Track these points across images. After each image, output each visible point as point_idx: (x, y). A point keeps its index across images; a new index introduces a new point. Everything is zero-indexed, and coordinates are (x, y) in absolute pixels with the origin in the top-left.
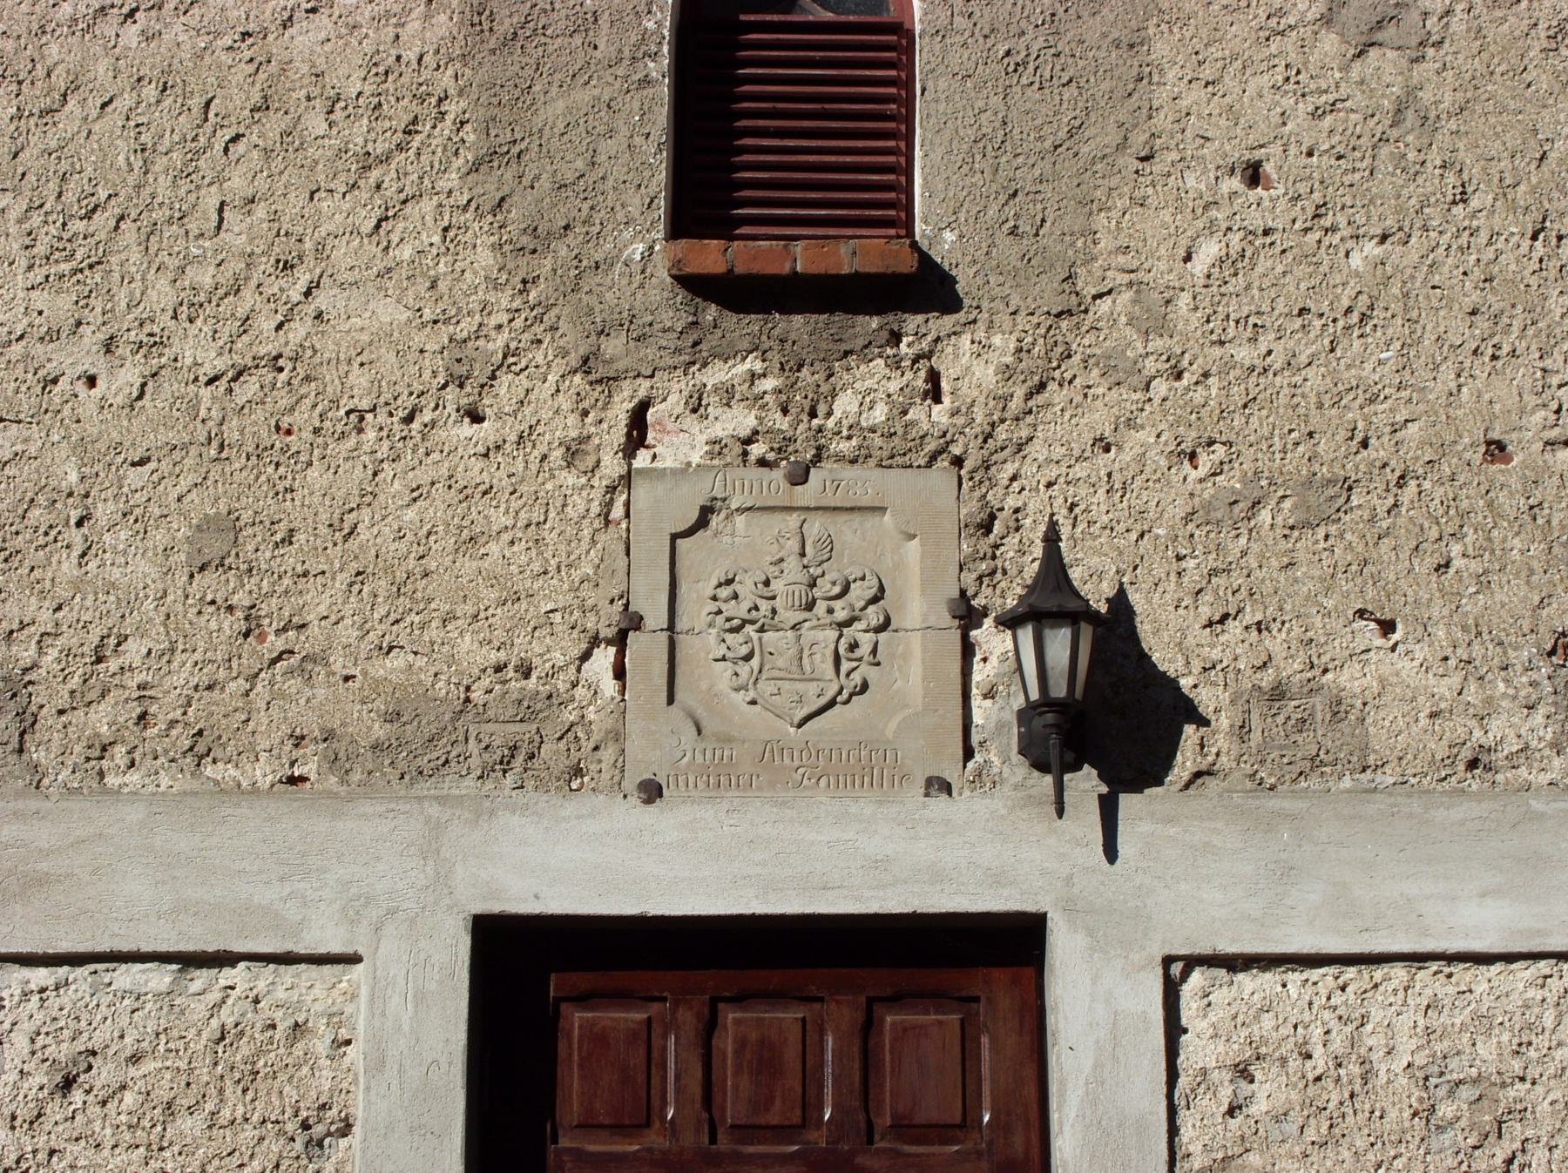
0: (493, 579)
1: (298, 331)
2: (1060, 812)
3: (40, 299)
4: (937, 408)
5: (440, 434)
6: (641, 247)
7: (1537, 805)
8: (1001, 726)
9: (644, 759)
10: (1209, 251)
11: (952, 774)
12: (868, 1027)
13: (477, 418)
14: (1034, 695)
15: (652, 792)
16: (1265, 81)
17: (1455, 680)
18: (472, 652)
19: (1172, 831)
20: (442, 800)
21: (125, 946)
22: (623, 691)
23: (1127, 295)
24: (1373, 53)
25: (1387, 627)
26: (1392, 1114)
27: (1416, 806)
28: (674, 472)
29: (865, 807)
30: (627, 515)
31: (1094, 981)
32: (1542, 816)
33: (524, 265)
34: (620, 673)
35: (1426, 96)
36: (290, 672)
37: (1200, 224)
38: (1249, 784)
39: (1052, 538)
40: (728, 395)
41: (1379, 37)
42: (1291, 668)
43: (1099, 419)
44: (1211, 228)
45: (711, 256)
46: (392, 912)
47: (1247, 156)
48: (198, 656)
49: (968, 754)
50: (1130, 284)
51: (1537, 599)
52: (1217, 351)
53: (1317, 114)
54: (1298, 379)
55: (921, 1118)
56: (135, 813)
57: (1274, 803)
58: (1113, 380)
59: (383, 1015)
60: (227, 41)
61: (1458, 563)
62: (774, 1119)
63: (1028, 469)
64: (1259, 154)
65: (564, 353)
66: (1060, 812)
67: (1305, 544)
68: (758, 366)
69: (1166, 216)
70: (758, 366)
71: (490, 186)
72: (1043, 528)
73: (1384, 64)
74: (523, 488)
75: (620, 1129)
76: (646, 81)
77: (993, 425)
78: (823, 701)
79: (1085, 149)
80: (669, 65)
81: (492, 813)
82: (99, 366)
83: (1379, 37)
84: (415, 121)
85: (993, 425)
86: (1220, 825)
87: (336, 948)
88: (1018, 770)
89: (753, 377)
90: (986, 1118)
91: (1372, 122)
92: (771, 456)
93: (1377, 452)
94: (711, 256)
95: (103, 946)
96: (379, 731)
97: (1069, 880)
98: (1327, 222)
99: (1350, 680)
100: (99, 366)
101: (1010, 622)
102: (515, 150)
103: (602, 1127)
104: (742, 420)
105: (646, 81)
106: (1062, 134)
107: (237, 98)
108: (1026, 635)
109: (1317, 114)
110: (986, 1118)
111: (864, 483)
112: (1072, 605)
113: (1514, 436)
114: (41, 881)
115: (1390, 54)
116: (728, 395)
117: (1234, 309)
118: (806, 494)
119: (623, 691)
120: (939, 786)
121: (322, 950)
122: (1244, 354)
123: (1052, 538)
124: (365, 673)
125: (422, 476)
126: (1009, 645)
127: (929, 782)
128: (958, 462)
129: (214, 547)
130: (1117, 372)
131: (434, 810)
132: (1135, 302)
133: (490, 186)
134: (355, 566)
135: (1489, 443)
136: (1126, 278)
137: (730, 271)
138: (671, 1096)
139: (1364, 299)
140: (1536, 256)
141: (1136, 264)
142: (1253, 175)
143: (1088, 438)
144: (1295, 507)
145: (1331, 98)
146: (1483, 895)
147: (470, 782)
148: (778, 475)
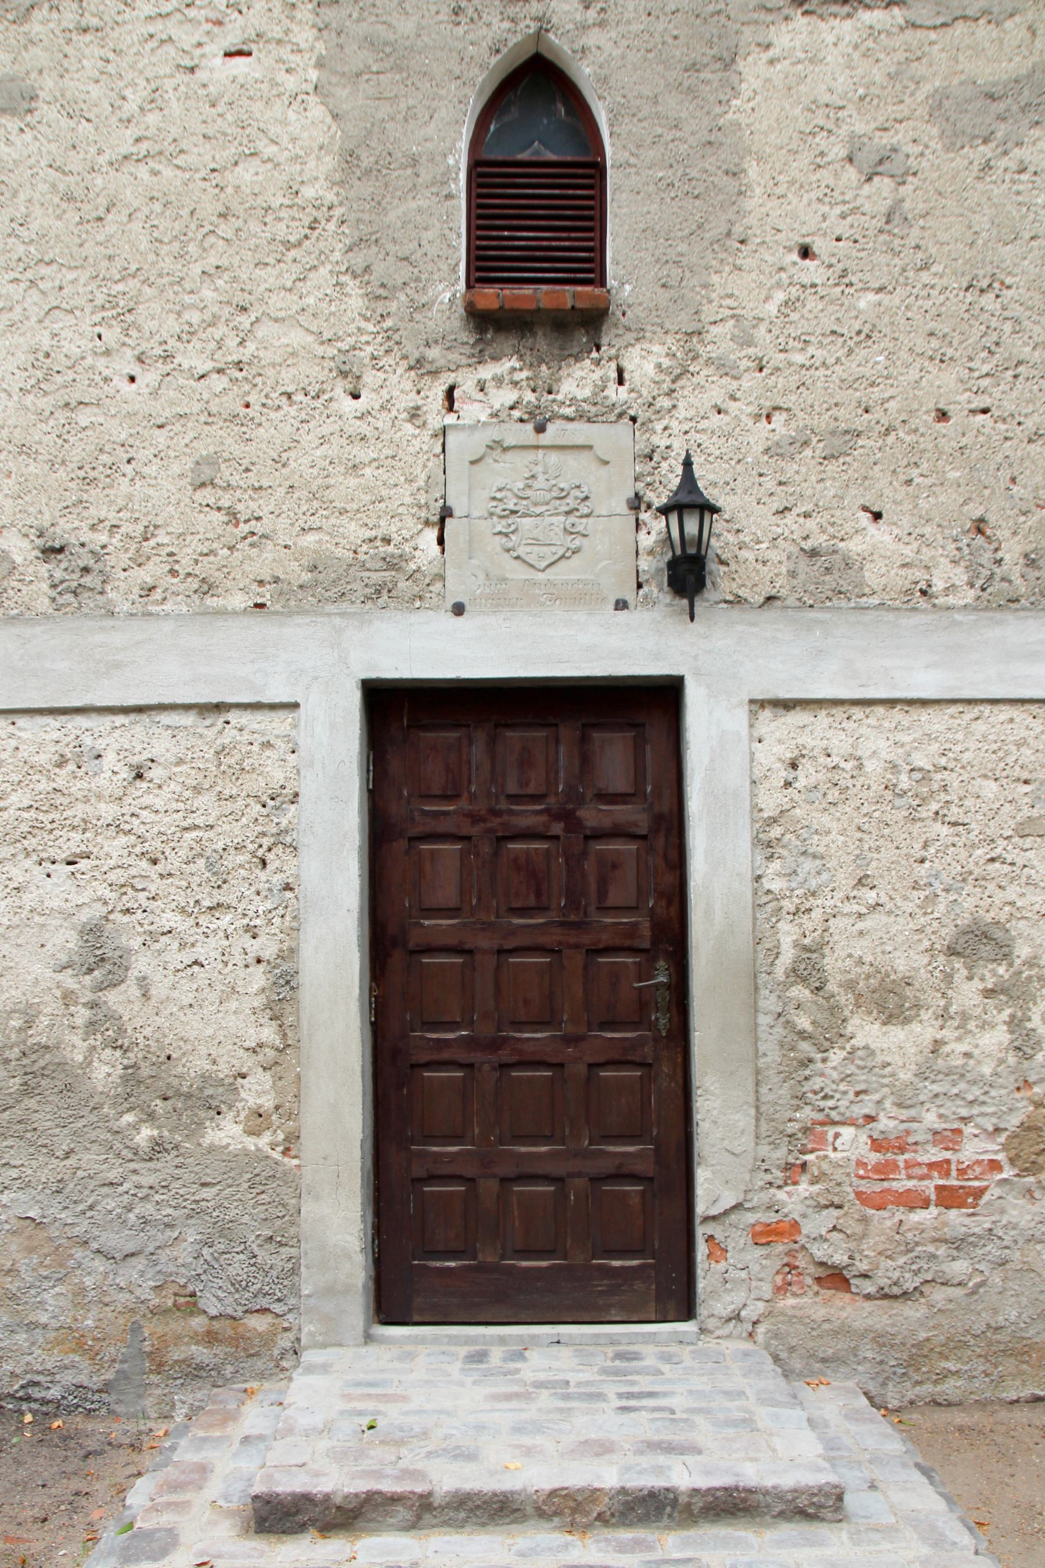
0: (367, 489)
1: (251, 347)
2: (692, 619)
3: (94, 317)
4: (621, 388)
5: (334, 405)
6: (448, 295)
7: (958, 617)
8: (659, 570)
9: (456, 592)
10: (780, 296)
11: (630, 596)
12: (584, 739)
13: (356, 396)
14: (678, 552)
15: (459, 610)
16: (813, 195)
17: (915, 545)
18: (355, 531)
19: (754, 630)
20: (342, 615)
21: (166, 700)
22: (443, 552)
23: (732, 322)
24: (876, 179)
25: (877, 516)
26: (874, 788)
27: (891, 616)
28: (470, 427)
29: (580, 616)
30: (444, 451)
31: (710, 714)
32: (961, 623)
33: (381, 307)
34: (441, 541)
35: (907, 205)
36: (252, 545)
37: (773, 281)
38: (798, 604)
39: (688, 464)
40: (499, 381)
41: (880, 169)
42: (819, 540)
43: (716, 394)
44: (779, 285)
45: (491, 296)
46: (316, 678)
47: (801, 241)
48: (200, 536)
49: (639, 586)
50: (733, 316)
51: (961, 501)
52: (782, 356)
53: (843, 216)
54: (829, 373)
55: (611, 791)
56: (168, 626)
57: (812, 614)
58: (721, 372)
59: (312, 736)
60: (202, 174)
61: (917, 480)
62: (531, 790)
63: (674, 424)
64: (808, 240)
65: (405, 357)
66: (692, 619)
67: (832, 467)
68: (517, 365)
69: (754, 275)
70: (517, 365)
71: (358, 260)
72: (683, 457)
73: (883, 184)
74: (384, 437)
75: (446, 798)
76: (449, 196)
77: (654, 398)
78: (556, 557)
79: (707, 236)
80: (484, 81)
81: (371, 621)
82: (136, 370)
83: (880, 169)
84: (316, 221)
85: (654, 398)
86: (781, 627)
87: (285, 699)
88: (666, 597)
89: (514, 369)
90: (649, 789)
91: (874, 221)
92: (526, 417)
93: (877, 414)
94: (491, 296)
95: (154, 701)
96: (306, 577)
97: (696, 657)
98: (846, 280)
99: (854, 546)
100: (136, 370)
101: (665, 511)
102: (374, 237)
103: (436, 796)
104: (509, 396)
105: (449, 196)
106: (694, 227)
107: (209, 209)
108: (674, 519)
109: (843, 216)
110: (649, 789)
111: (579, 432)
112: (699, 501)
113: (952, 407)
114: (117, 665)
115: (886, 180)
116: (499, 381)
117: (791, 330)
118: (545, 439)
119: (443, 552)
120: (621, 605)
121: (277, 701)
122: (799, 358)
123: (688, 464)
124: (295, 544)
125: (326, 430)
126: (664, 523)
127: (617, 602)
128: (634, 419)
129: (207, 473)
130: (726, 369)
131: (337, 621)
132: (735, 327)
133: (358, 260)
134: (288, 484)
135: (938, 410)
136: (731, 312)
137: (501, 308)
138: (474, 779)
139: (868, 326)
140: (968, 301)
141: (736, 304)
142: (806, 252)
143: (708, 405)
144: (825, 446)
145: (851, 206)
146: (927, 667)
147: (358, 604)
148: (530, 427)
